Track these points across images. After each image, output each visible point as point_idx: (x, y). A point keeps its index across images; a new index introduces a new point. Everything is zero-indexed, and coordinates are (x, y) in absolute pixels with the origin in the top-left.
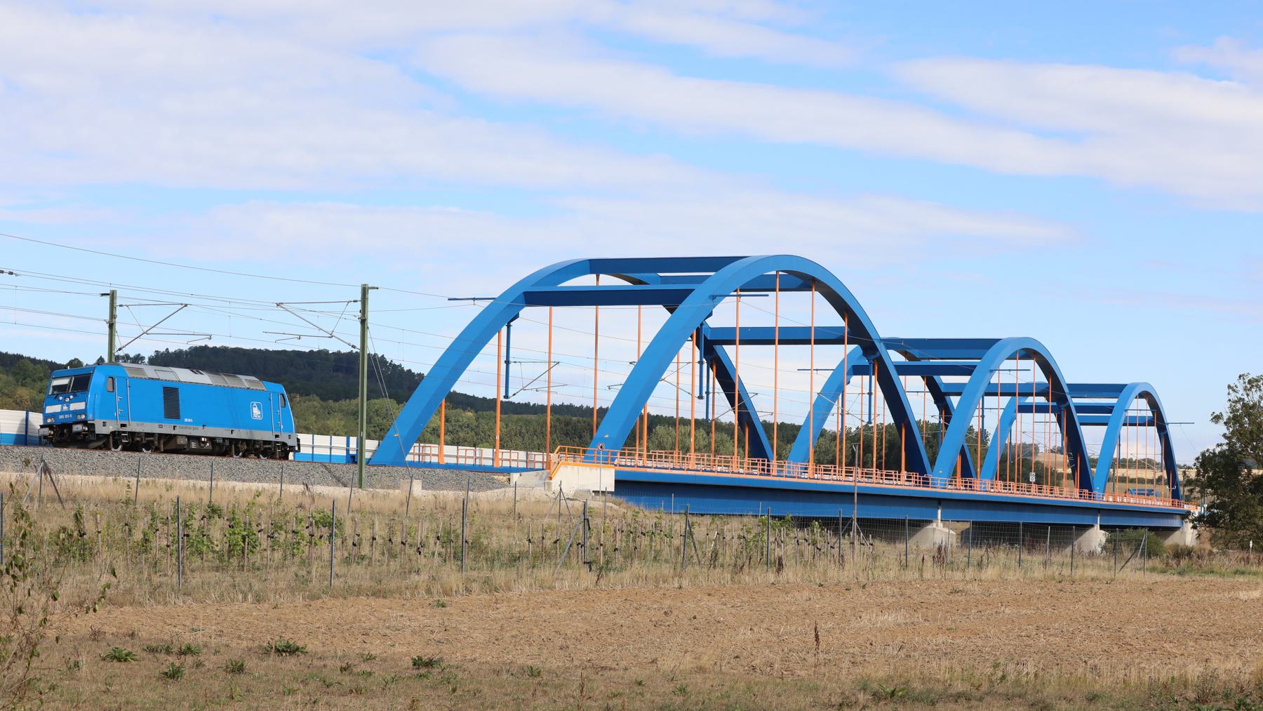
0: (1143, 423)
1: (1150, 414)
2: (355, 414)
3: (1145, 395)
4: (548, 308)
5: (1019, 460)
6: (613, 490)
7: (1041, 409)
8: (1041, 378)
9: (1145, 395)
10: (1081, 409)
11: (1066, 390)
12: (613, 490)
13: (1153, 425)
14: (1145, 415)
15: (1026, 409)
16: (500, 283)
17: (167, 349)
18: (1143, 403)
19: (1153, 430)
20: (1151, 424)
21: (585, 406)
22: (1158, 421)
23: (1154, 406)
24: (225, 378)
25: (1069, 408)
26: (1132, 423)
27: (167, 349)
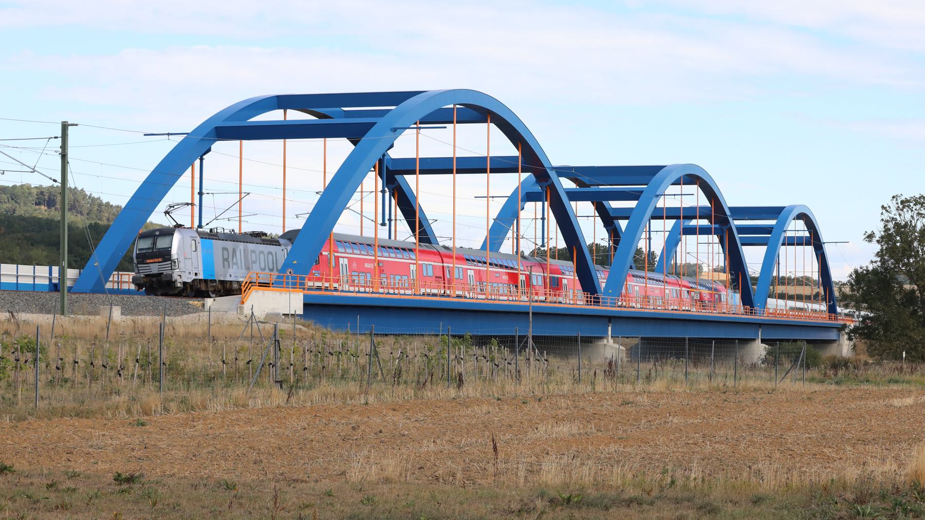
0: (800, 242)
1: (807, 234)
3: (801, 216)
7: (704, 231)
11: (728, 213)
18: (801, 224)
19: (810, 249)
20: (808, 244)
22: (814, 240)
25: (730, 229)
26: (791, 242)
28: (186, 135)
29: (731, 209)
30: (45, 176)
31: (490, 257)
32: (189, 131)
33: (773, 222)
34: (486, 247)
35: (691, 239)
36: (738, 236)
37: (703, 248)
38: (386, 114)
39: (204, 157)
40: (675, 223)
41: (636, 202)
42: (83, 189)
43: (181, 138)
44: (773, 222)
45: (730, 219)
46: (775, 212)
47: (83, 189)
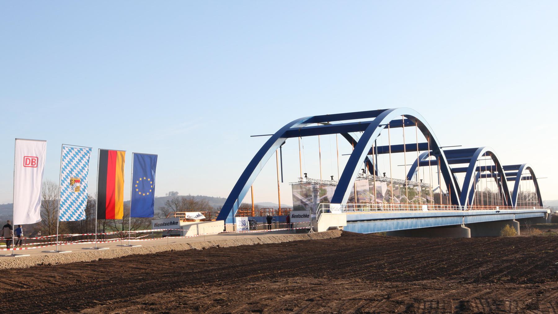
0: (528, 178)
1: (530, 175)
2: (188, 217)
3: (528, 168)
4: (336, 134)
5: (499, 202)
6: (224, 221)
7: (489, 176)
8: (493, 164)
9: (528, 168)
10: (507, 175)
11: (502, 168)
12: (224, 221)
13: (532, 179)
14: (525, 176)
15: (484, 176)
16: (274, 130)
17: (220, 197)
18: (528, 171)
19: (532, 181)
20: (531, 179)
21: (199, 195)
22: (533, 177)
23: (532, 172)
24: (107, 204)
25: (503, 174)
26: (524, 178)
27: (220, 197)
28: (272, 136)
29: (503, 166)
30: (35, 140)
31: (439, 162)
32: (274, 134)
33: (517, 171)
34: (291, 226)
35: (484, 179)
36: (506, 177)
37: (489, 183)
38: (368, 126)
39: (282, 146)
40: (466, 175)
41: (469, 164)
42: (333, 176)
43: (272, 136)
44: (517, 171)
45: (503, 170)
46: (518, 167)
47: (333, 176)
